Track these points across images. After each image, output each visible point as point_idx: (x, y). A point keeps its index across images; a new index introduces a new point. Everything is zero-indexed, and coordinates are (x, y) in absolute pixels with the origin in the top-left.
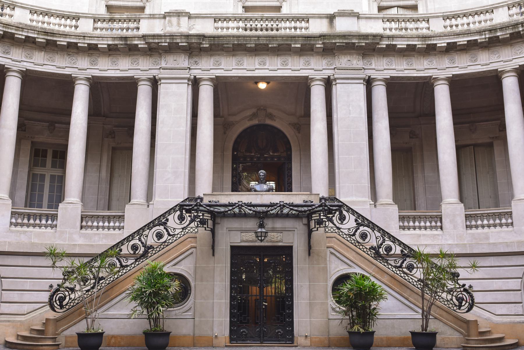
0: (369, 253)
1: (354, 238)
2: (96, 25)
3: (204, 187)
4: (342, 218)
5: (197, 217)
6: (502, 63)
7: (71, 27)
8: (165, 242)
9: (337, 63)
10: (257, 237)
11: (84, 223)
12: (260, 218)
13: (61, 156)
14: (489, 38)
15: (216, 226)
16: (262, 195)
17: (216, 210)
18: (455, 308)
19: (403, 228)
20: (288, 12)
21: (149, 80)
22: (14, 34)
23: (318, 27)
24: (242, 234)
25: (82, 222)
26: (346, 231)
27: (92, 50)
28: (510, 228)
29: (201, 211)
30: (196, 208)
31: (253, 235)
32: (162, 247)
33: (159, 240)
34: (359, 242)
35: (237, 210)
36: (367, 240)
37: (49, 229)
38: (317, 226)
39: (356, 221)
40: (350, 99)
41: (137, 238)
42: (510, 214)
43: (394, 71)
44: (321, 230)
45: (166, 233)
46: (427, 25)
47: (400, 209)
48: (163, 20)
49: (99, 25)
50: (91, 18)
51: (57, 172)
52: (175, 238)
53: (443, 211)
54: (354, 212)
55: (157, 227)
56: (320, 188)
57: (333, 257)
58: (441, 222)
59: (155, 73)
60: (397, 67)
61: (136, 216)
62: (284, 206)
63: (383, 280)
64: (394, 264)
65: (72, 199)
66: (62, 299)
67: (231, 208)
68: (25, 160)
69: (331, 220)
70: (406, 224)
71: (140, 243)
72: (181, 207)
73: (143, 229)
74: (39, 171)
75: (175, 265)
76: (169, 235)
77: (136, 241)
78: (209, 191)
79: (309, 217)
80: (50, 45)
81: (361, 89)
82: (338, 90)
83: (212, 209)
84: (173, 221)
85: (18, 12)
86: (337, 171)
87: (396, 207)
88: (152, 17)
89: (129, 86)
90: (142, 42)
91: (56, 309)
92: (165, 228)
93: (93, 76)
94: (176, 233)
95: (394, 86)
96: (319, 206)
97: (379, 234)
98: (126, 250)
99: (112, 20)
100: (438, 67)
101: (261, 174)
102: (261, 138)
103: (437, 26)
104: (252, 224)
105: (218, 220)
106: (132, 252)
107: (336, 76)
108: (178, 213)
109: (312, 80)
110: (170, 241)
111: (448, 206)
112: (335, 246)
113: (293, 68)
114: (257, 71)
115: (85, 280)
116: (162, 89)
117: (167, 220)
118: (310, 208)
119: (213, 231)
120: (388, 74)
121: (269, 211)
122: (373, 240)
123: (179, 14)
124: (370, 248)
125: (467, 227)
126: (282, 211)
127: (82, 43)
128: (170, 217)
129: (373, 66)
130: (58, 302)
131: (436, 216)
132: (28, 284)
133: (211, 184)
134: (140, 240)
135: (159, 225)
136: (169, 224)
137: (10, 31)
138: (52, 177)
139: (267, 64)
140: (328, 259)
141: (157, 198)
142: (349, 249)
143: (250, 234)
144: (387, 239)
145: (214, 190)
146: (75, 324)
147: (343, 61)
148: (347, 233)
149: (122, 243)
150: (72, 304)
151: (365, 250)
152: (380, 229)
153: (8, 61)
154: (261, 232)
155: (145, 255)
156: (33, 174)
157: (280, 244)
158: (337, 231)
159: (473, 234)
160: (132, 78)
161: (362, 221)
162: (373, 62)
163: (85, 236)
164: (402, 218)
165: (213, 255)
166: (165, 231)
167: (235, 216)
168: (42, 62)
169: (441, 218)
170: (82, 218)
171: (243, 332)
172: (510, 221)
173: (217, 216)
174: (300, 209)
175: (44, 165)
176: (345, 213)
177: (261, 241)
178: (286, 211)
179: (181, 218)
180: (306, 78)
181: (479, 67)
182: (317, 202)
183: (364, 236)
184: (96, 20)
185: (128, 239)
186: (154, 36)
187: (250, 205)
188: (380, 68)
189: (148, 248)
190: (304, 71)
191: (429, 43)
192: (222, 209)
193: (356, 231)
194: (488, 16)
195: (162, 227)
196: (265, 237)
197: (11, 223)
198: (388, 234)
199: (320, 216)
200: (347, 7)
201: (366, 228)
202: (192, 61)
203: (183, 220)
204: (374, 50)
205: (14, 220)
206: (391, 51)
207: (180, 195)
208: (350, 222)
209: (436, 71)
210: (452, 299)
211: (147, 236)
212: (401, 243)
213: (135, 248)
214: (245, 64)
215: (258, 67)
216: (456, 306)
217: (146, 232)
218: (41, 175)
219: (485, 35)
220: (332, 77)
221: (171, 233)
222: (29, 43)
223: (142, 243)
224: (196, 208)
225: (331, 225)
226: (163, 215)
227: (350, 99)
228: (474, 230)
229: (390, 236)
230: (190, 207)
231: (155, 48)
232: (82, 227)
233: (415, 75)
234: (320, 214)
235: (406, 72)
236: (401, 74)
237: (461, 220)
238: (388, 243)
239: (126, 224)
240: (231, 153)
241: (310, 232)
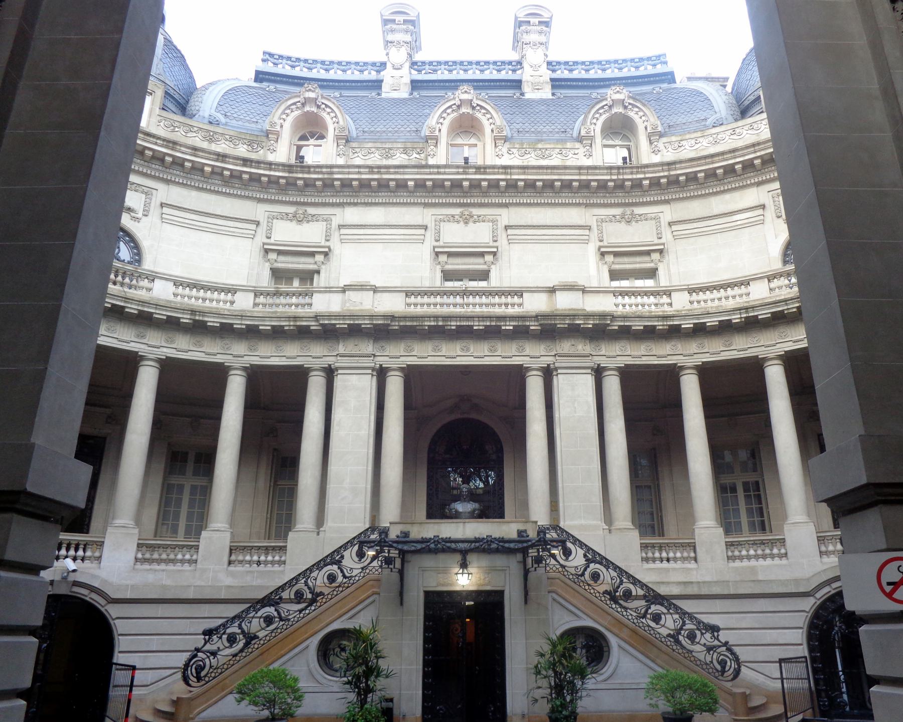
0: (603, 599)
1: (582, 578)
2: (258, 300)
3: (390, 513)
4: (567, 553)
6: (763, 348)
7: (225, 302)
9: (558, 348)
11: (233, 558)
13: (206, 460)
14: (746, 318)
15: (406, 565)
18: (717, 674)
19: (646, 560)
20: (498, 285)
22: (152, 313)
23: (535, 304)
25: (230, 555)
26: (573, 571)
27: (252, 333)
28: (784, 561)
34: (589, 585)
37: (186, 567)
39: (585, 556)
40: (575, 394)
41: (303, 581)
42: (783, 541)
43: (629, 358)
44: (541, 571)
45: (340, 574)
46: (669, 301)
47: (642, 535)
48: (340, 295)
49: (261, 299)
50: (251, 291)
51: (200, 482)
53: (696, 537)
54: (582, 545)
55: (329, 567)
56: (540, 514)
57: (556, 606)
58: (695, 552)
59: (330, 360)
60: (633, 353)
61: (303, 548)
63: (622, 635)
65: (219, 525)
66: (199, 669)
68: (160, 467)
70: (650, 555)
73: (310, 569)
74: (175, 480)
75: (351, 618)
76: (344, 576)
79: (524, 551)
80: (198, 328)
81: (588, 381)
82: (561, 382)
84: (350, 560)
85: (158, 284)
86: (560, 485)
87: (636, 533)
88: (329, 290)
89: (296, 378)
90: (313, 323)
91: (190, 682)
92: (339, 568)
93: (251, 365)
94: (354, 574)
97: (615, 574)
99: (277, 294)
100: (684, 353)
101: (464, 490)
102: (464, 435)
103: (680, 302)
105: (408, 557)
107: (557, 365)
108: (356, 547)
109: (528, 369)
111: (703, 531)
112: (560, 591)
113: (503, 354)
114: (458, 359)
115: (232, 640)
116: (339, 381)
117: (342, 557)
120: (622, 362)
123: (361, 287)
124: (604, 593)
125: (729, 558)
127: (238, 324)
128: (346, 554)
129: (603, 353)
130: (194, 670)
132: (155, 643)
135: (332, 564)
136: (344, 562)
137: (146, 309)
138: (194, 488)
139: (472, 350)
140: (550, 608)
141: (330, 523)
142: (577, 594)
144: (625, 580)
146: (216, 702)
147: (566, 346)
148: (574, 572)
149: (282, 588)
150: (213, 675)
152: (616, 568)
153: (143, 346)
156: (168, 484)
158: (560, 569)
159: (737, 569)
160: (301, 367)
161: (592, 557)
162: (603, 347)
163: (232, 574)
164: (644, 547)
165: (402, 604)
166: (339, 571)
168: (187, 348)
169: (695, 547)
170: (231, 550)
171: (441, 709)
172: (783, 551)
174: (507, 545)
175: (183, 473)
176: (569, 545)
178: (494, 546)
179: (361, 555)
180: (520, 367)
181: (735, 352)
182: (532, 534)
184: (257, 293)
185: (291, 583)
186: (330, 316)
188: (611, 354)
189: (316, 596)
190: (518, 358)
191: (672, 323)
193: (585, 570)
194: (743, 290)
195: (335, 567)
197: (136, 559)
198: (626, 573)
199: (538, 552)
200: (570, 279)
201: (598, 566)
202: (377, 346)
203: (363, 557)
204: (604, 331)
205: (140, 556)
206: (626, 334)
207: (358, 524)
209: (681, 357)
210: (712, 662)
214: (444, 349)
215: (460, 353)
216: (718, 671)
217: (314, 574)
218: (178, 485)
219: (740, 314)
221: (347, 575)
222: (171, 325)
225: (553, 562)
226: (337, 551)
227: (575, 394)
228: (738, 564)
229: (629, 576)
230: (372, 539)
231: (328, 332)
232: (230, 563)
233: (656, 362)
234: (538, 550)
235: (644, 358)
236: (638, 362)
237: (720, 549)
239: (288, 557)
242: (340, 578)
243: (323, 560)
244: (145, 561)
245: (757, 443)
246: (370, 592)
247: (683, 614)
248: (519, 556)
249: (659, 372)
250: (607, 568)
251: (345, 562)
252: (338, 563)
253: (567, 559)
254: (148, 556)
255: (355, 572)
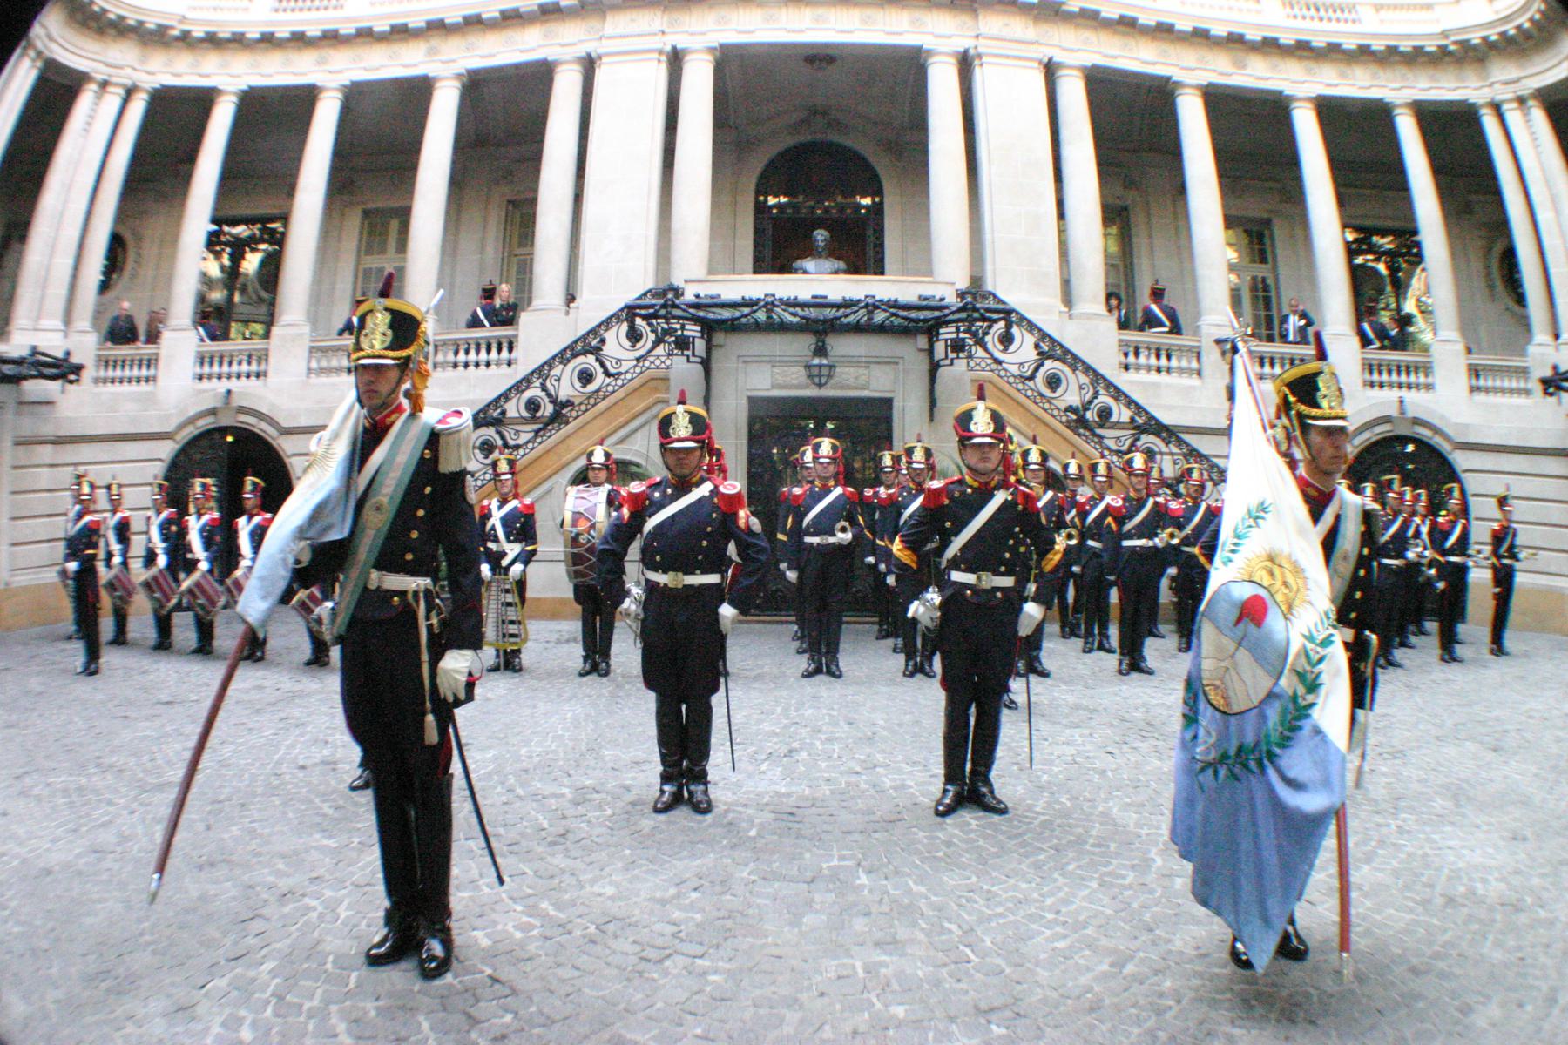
1: (1031, 384)
4: (1006, 340)
5: (666, 332)
8: (598, 391)
10: (810, 376)
12: (816, 333)
15: (716, 353)
16: (818, 282)
17: (711, 316)
21: (580, 60)
24: (776, 370)
26: (1014, 370)
29: (679, 318)
30: (663, 312)
31: (802, 371)
32: (592, 401)
33: (584, 386)
34: (1041, 395)
35: (761, 316)
36: (1060, 391)
38: (952, 355)
39: (1037, 346)
41: (537, 384)
44: (961, 365)
45: (600, 370)
52: (620, 382)
54: (1032, 327)
55: (581, 359)
56: (946, 280)
59: (592, 47)
61: (542, 332)
62: (876, 307)
64: (1114, 447)
67: (746, 310)
69: (981, 343)
71: (543, 394)
72: (630, 312)
73: (549, 364)
75: (621, 441)
76: (607, 374)
77: (534, 392)
78: (701, 273)
83: (701, 314)
84: (615, 344)
89: (539, 77)
94: (623, 370)
95: (1100, 83)
96: (960, 310)
98: (514, 409)
104: (802, 345)
106: (525, 414)
110: (610, 389)
117: (603, 341)
118: (937, 313)
119: (706, 364)
121: (838, 318)
122: (1072, 393)
124: (1066, 410)
126: (870, 319)
128: (610, 336)
131: (1190, 349)
133: (706, 260)
134: (543, 388)
135: (585, 353)
136: (606, 350)
143: (794, 369)
145: (711, 272)
149: (506, 396)
151: (1056, 413)
152: (1088, 369)
154: (820, 366)
155: (557, 418)
157: (865, 394)
158: (994, 366)
161: (1050, 348)
166: (597, 365)
167: (758, 328)
173: (720, 324)
174: (913, 314)
177: (820, 385)
178: (879, 317)
179: (634, 336)
183: (1054, 382)
185: (518, 387)
187: (793, 304)
192: (726, 314)
193: (1037, 369)
195: (591, 359)
196: (830, 377)
197: (310, 370)
201: (1058, 365)
208: (1024, 349)
211: (558, 380)
212: (1130, 402)
213: (533, 406)
217: (556, 372)
220: (972, 52)
221: (612, 371)
223: (549, 395)
224: (663, 312)
225: (980, 353)
226: (594, 331)
229: (1109, 385)
230: (656, 311)
238: (1104, 399)
240: (751, 199)
241: (934, 367)
242: (600, 379)
243: (571, 347)
244: (322, 371)
245: (1267, 223)
246: (650, 401)
247: (1194, 454)
248: (922, 341)
249: (1138, 86)
250: (1074, 370)
251: (607, 350)
252: (596, 351)
253: (1005, 349)
254: (324, 364)
255: (625, 366)
